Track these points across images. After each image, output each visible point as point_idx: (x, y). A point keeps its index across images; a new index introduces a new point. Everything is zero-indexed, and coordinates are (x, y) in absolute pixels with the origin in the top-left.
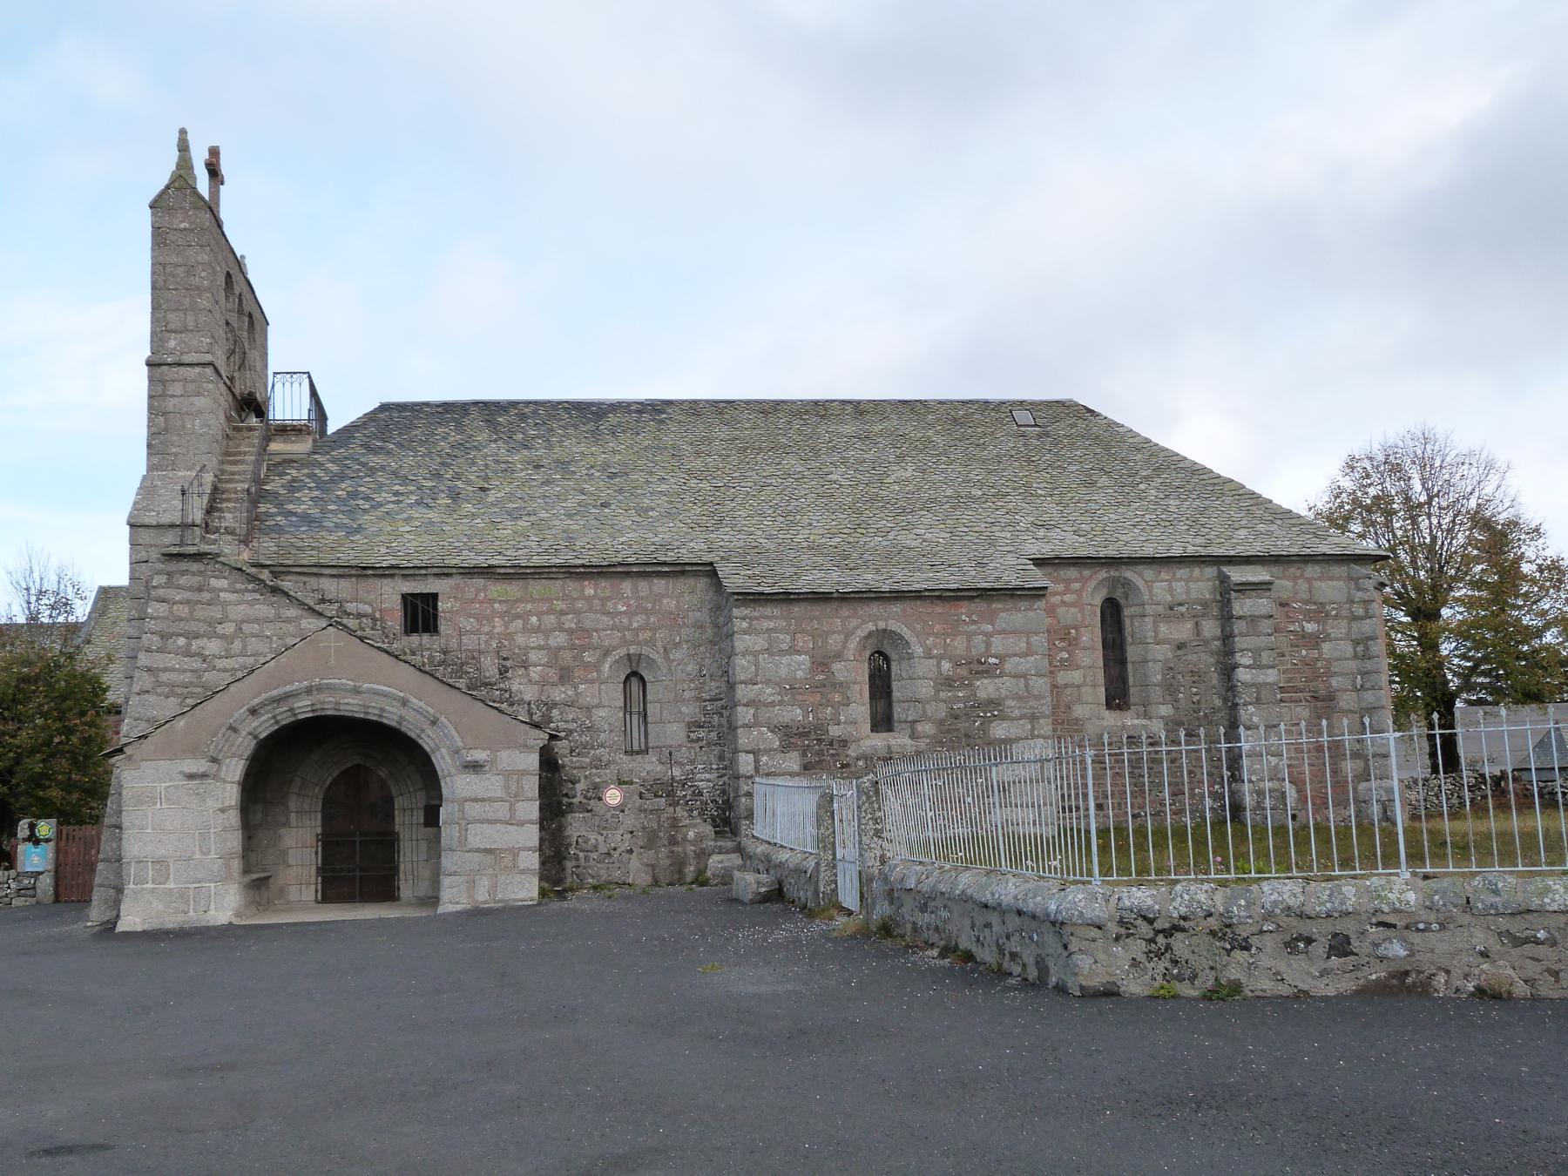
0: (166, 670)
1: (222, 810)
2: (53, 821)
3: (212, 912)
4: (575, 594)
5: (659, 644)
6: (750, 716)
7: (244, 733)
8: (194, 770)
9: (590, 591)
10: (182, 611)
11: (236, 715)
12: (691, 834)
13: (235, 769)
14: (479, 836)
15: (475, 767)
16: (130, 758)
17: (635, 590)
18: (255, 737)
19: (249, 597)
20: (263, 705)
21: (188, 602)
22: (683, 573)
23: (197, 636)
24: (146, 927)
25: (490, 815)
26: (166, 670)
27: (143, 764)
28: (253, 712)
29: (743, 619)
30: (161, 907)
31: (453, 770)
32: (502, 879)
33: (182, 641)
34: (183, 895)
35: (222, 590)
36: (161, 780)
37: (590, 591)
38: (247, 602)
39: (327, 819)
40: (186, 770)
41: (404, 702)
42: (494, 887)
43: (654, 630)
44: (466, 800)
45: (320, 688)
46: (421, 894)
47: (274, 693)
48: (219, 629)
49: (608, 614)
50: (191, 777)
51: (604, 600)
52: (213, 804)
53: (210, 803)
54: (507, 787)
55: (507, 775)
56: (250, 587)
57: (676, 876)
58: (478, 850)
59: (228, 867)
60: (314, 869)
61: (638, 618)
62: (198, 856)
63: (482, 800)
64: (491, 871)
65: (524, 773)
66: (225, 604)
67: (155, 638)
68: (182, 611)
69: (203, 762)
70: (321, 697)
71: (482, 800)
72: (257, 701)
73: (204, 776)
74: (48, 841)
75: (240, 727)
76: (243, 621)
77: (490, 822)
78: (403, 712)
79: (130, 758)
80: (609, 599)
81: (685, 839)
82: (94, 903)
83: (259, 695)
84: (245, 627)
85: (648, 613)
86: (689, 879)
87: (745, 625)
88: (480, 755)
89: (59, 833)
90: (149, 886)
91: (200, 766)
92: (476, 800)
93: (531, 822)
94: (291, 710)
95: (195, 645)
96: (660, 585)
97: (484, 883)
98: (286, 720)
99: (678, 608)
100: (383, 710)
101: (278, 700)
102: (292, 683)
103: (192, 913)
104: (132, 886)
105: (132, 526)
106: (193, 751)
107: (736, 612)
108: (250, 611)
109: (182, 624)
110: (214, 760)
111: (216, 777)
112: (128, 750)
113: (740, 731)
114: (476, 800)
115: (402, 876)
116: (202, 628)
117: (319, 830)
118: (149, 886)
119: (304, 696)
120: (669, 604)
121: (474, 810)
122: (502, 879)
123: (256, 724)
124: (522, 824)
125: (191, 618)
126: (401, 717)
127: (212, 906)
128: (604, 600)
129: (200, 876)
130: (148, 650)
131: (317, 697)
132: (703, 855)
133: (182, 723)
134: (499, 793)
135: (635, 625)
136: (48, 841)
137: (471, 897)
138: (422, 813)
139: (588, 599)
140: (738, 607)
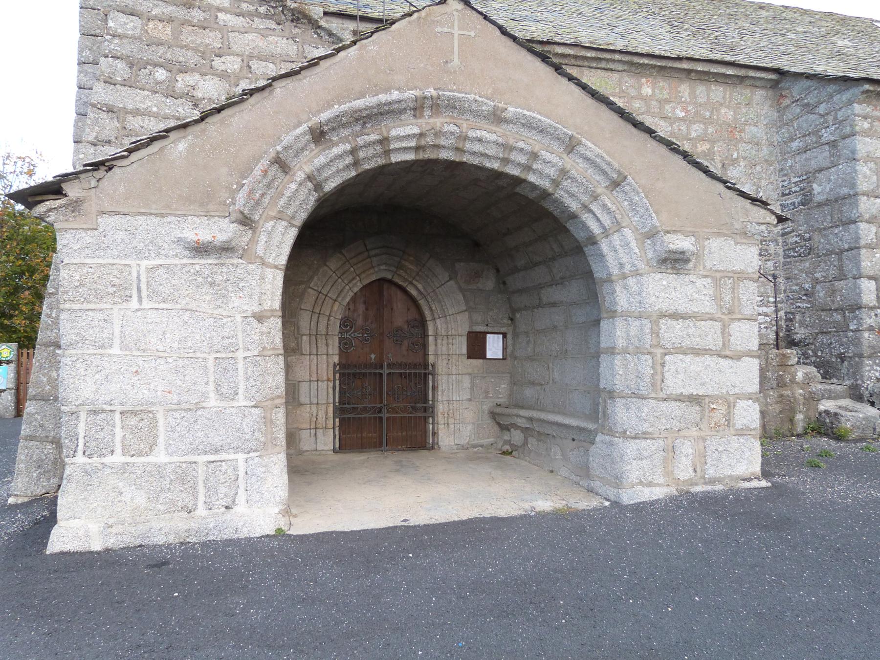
0: (137, 112)
1: (259, 318)
2: (14, 345)
3: (240, 508)
4: (633, 92)
5: (718, 159)
6: (872, 235)
7: (300, 176)
8: (205, 236)
9: (647, 90)
10: (165, 32)
11: (287, 139)
12: (800, 376)
13: (278, 241)
14: (683, 374)
15: (675, 262)
16: (76, 205)
17: (693, 95)
18: (318, 187)
19: (259, 23)
20: (337, 123)
21: (170, 20)
22: (742, 79)
23: (184, 70)
24: (112, 542)
25: (697, 342)
26: (137, 112)
27: (105, 222)
28: (319, 135)
29: (865, 118)
30: (141, 500)
31: (641, 265)
32: (713, 443)
33: (161, 74)
34: (184, 476)
35: (220, 10)
36: (138, 254)
37: (647, 90)
38: (257, 31)
39: (345, 345)
40: (190, 235)
41: (571, 146)
42: (702, 457)
43: (713, 142)
44: (663, 315)
45: (436, 105)
46: (464, 441)
47: (359, 104)
48: (217, 63)
49: (666, 118)
50: (200, 250)
51: (662, 102)
52: (241, 303)
53: (235, 301)
54: (717, 298)
55: (718, 278)
56: (263, 9)
57: (787, 426)
58: (679, 398)
59: (268, 421)
60: (331, 409)
61: (695, 127)
62: (213, 402)
63: (684, 317)
64: (694, 432)
65: (741, 276)
66: (225, 30)
67: (120, 65)
68: (165, 32)
69: (224, 223)
70: (438, 122)
71: (684, 317)
72: (325, 116)
73: (226, 249)
74: (8, 362)
75: (294, 163)
76: (251, 57)
77: (697, 352)
78: (569, 162)
79: (76, 205)
80: (667, 101)
81: (793, 381)
82: (20, 466)
83: (330, 106)
84: (255, 65)
85: (706, 122)
86: (800, 429)
87: (866, 125)
88: (682, 243)
89: (19, 355)
90: (118, 458)
91: (222, 230)
92: (676, 316)
93: (749, 354)
94: (384, 141)
95: (183, 82)
96: (718, 92)
97: (687, 449)
98: (371, 161)
99: (735, 119)
100: (535, 156)
101: (364, 118)
102: (387, 90)
103: (201, 511)
104: (80, 459)
105: (80, 88)
106: (204, 202)
107: (857, 108)
108: (261, 43)
109: (161, 50)
110: (246, 221)
111: (246, 254)
112: (72, 190)
113: (863, 251)
114: (676, 316)
115: (440, 419)
116: (192, 58)
117: (336, 359)
118: (118, 458)
119: (408, 117)
120: (726, 114)
121: (674, 332)
122: (713, 443)
123: (322, 160)
124: (737, 357)
125: (176, 43)
126: (564, 172)
127: (241, 497)
128: (662, 102)
129: (217, 441)
130: (109, 82)
131: (444, 123)
132: (812, 398)
133: (182, 146)
134: (708, 307)
135: (694, 134)
136: (8, 362)
137: (668, 473)
138: (464, 341)
139: (645, 99)
140: (860, 103)
